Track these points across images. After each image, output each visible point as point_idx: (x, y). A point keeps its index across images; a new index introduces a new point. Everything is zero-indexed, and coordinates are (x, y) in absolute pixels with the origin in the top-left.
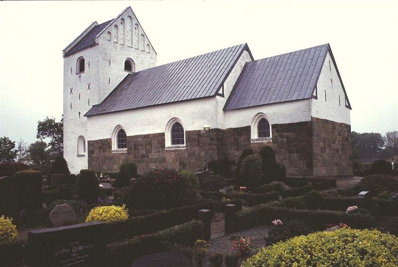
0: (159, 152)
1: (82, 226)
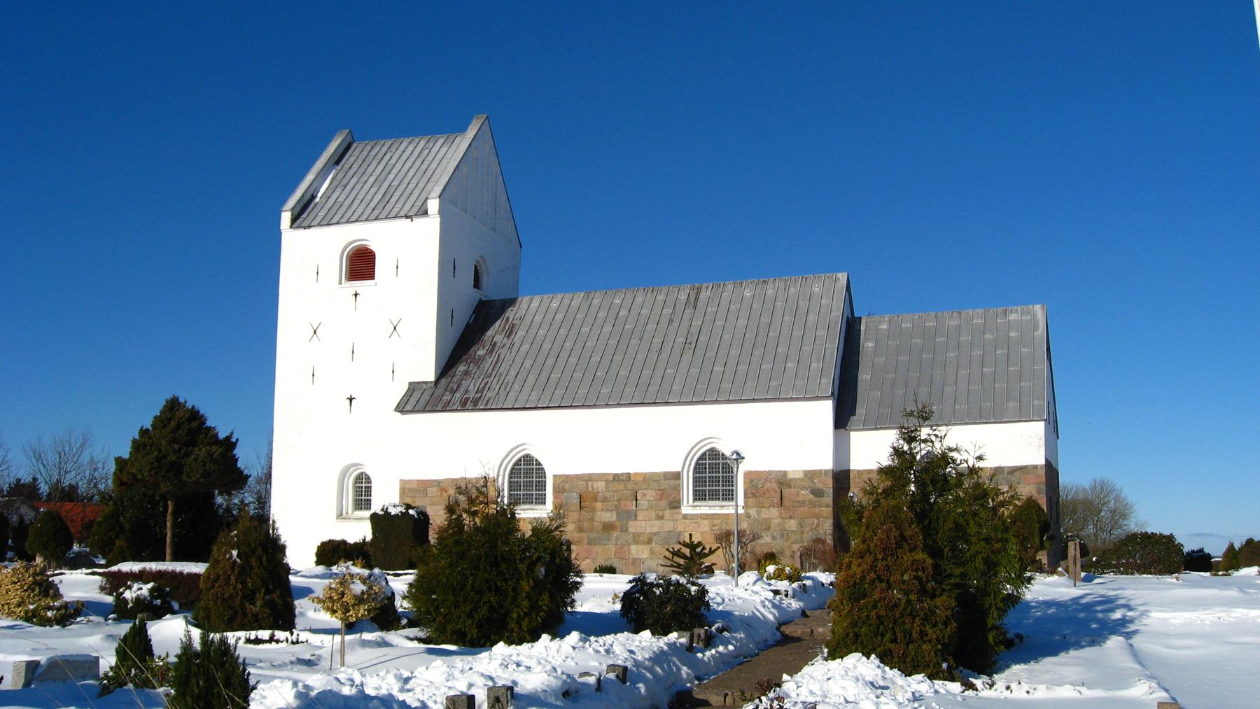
0: (662, 518)
1: (167, 556)
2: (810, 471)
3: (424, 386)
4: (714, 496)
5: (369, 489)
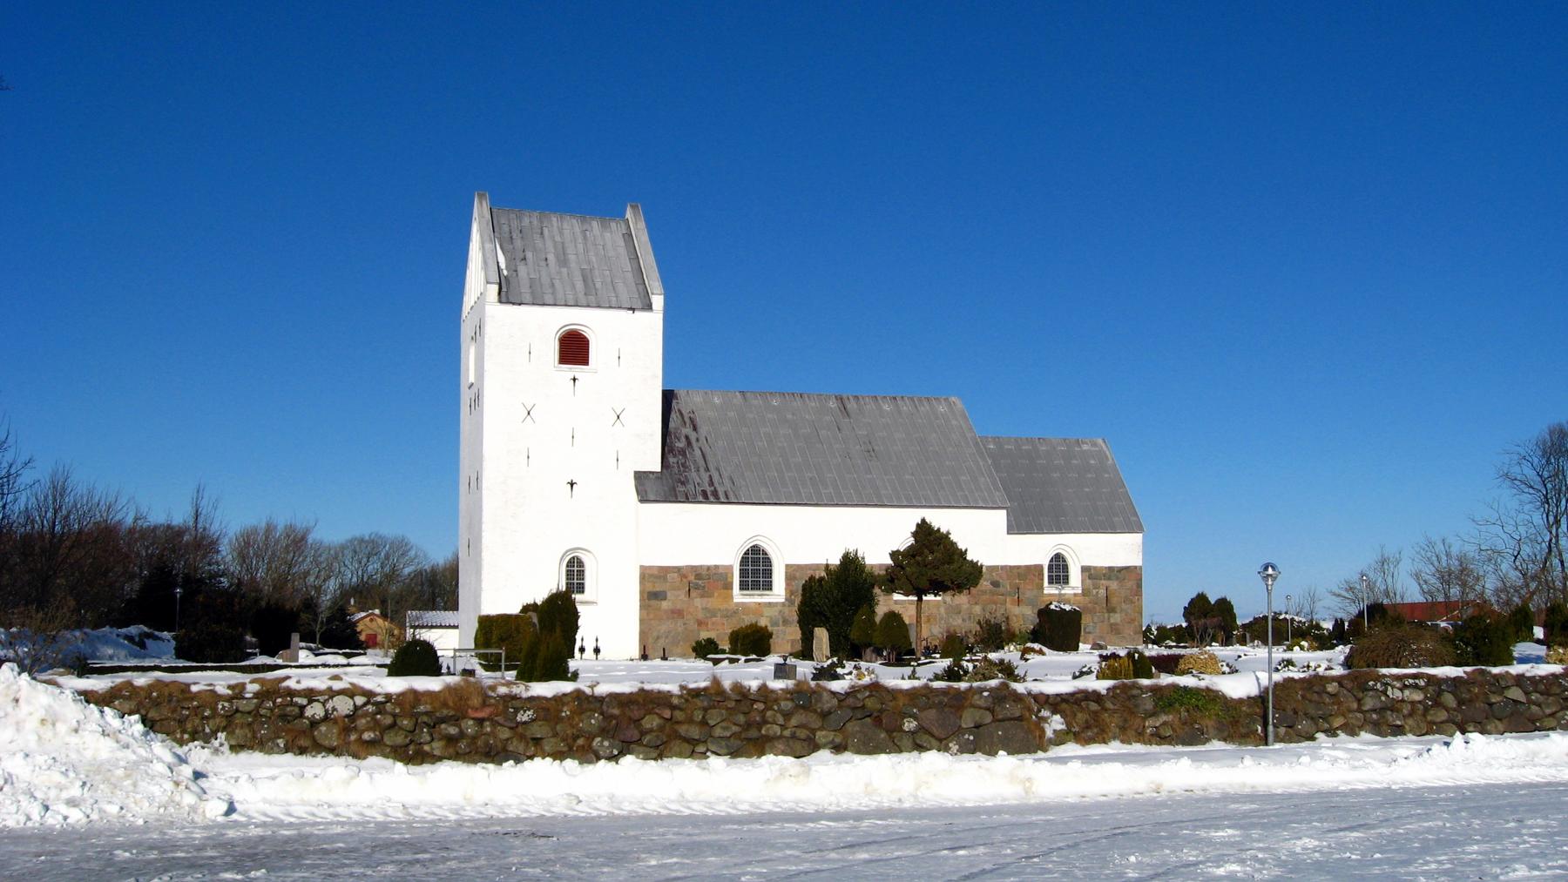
2: (990, 567)
3: (651, 475)
4: (756, 586)
5: (581, 573)
